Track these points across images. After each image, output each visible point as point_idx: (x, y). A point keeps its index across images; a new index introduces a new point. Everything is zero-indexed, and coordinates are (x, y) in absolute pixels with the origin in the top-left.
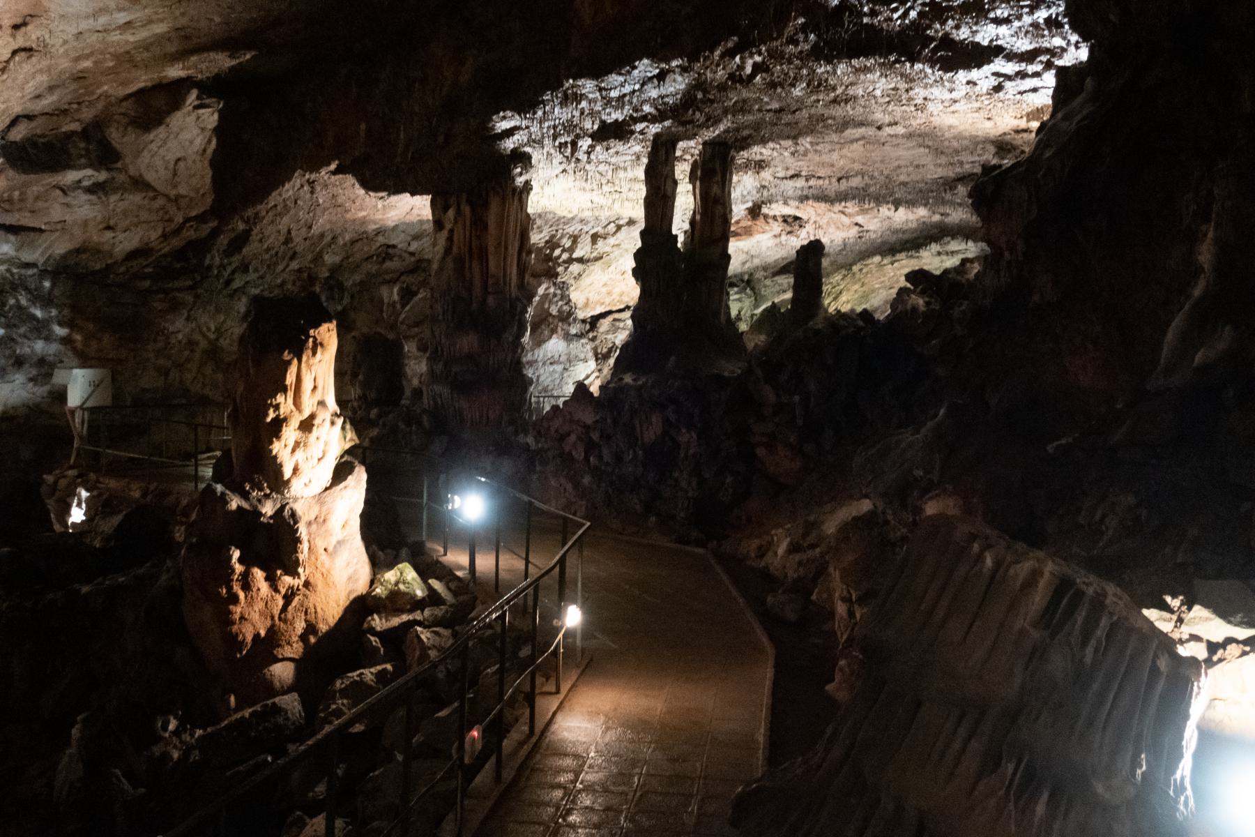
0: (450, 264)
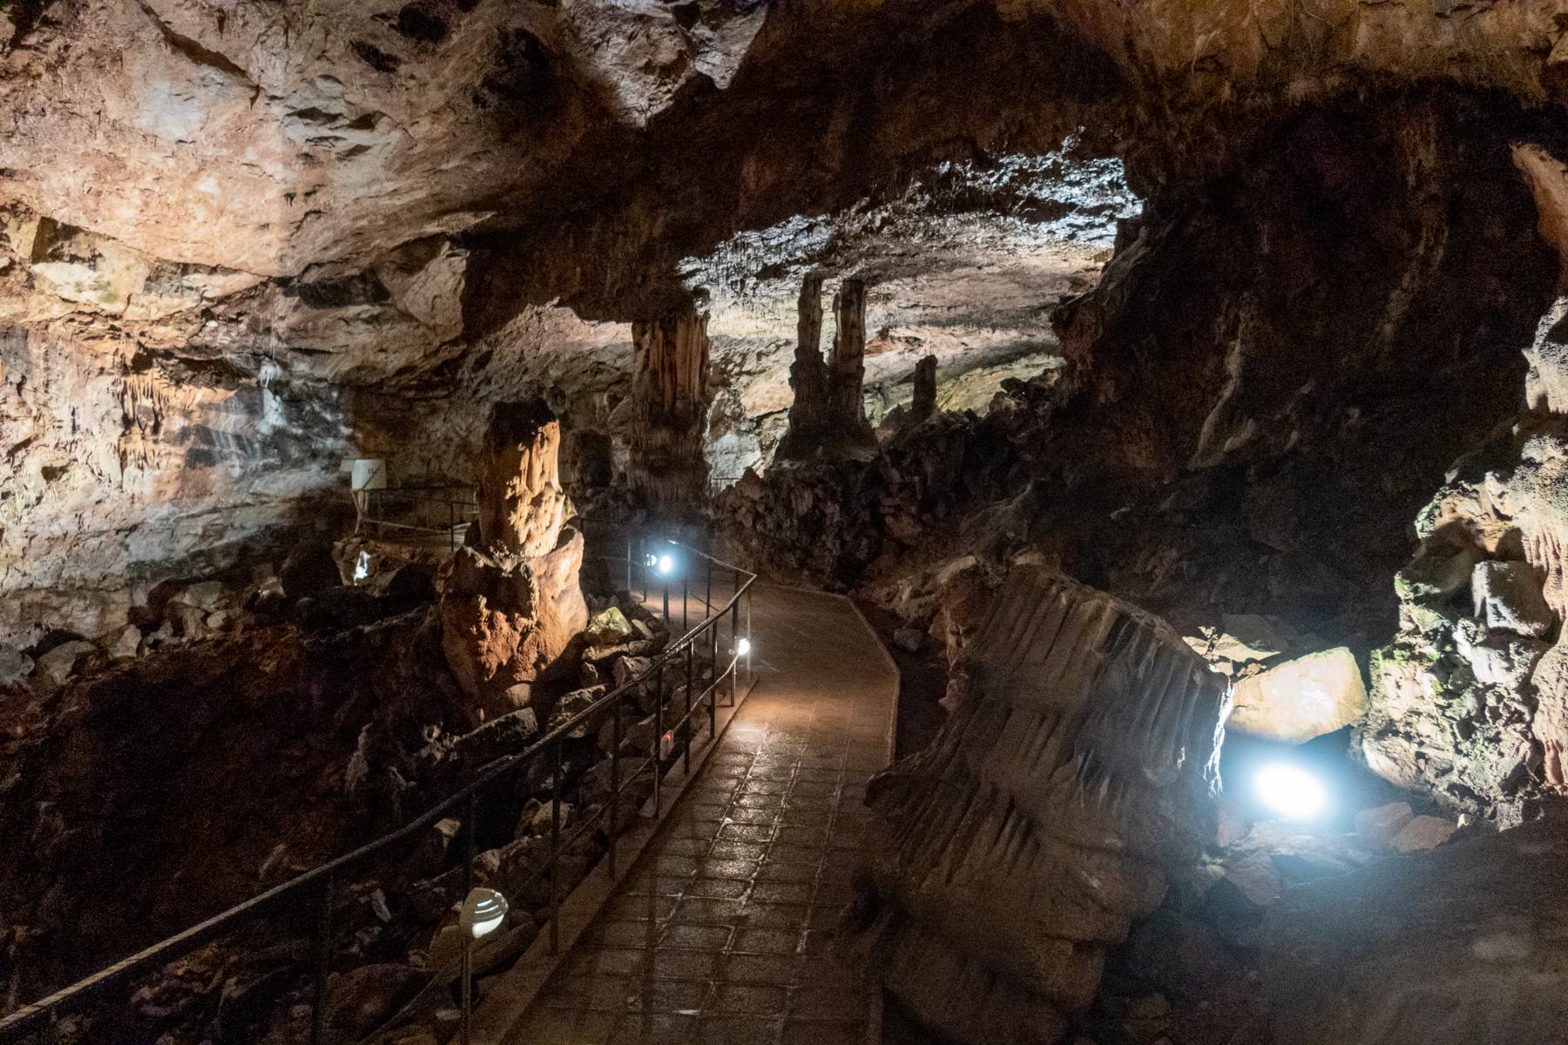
0: (647, 376)
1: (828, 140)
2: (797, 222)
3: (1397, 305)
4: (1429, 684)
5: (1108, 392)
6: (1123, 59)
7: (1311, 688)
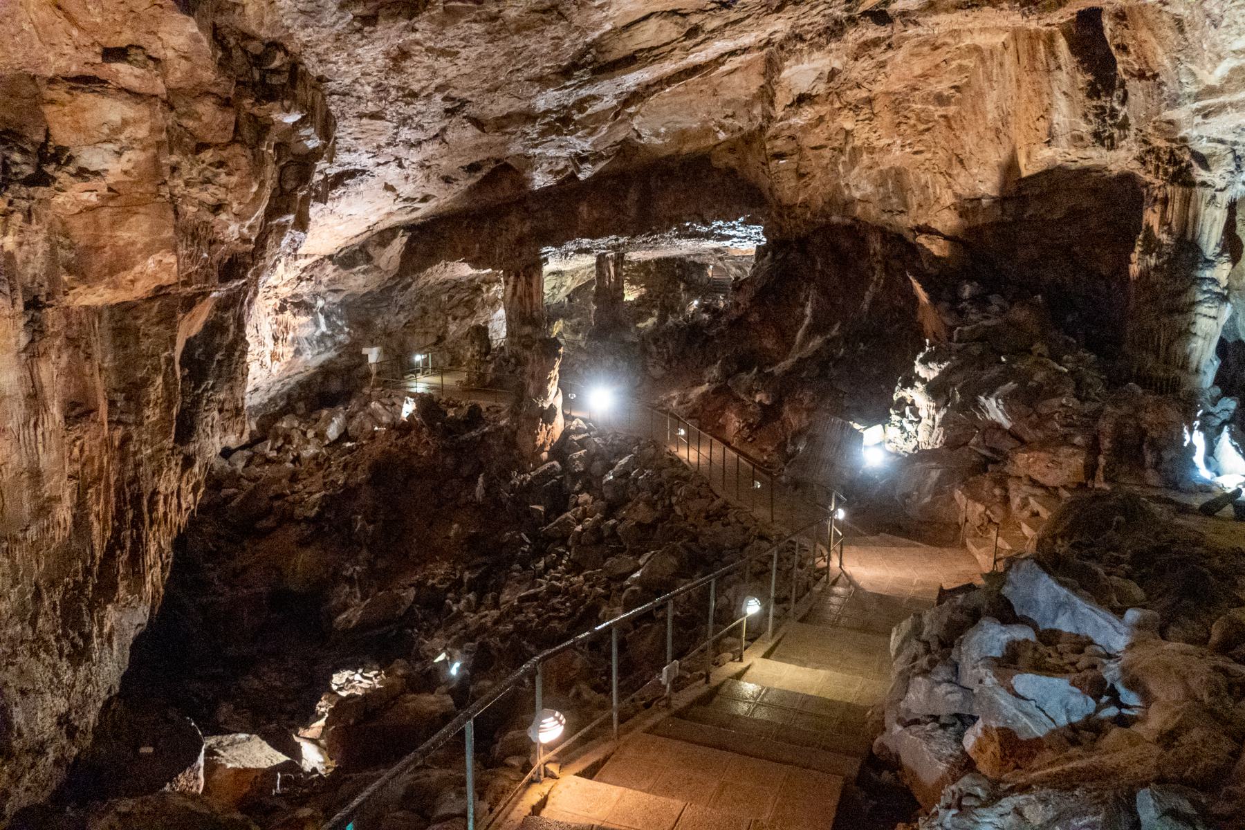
0: (516, 299)
1: (628, 203)
2: (613, 237)
3: (868, 297)
4: (899, 431)
5: (755, 317)
6: (768, 193)
7: (872, 435)
